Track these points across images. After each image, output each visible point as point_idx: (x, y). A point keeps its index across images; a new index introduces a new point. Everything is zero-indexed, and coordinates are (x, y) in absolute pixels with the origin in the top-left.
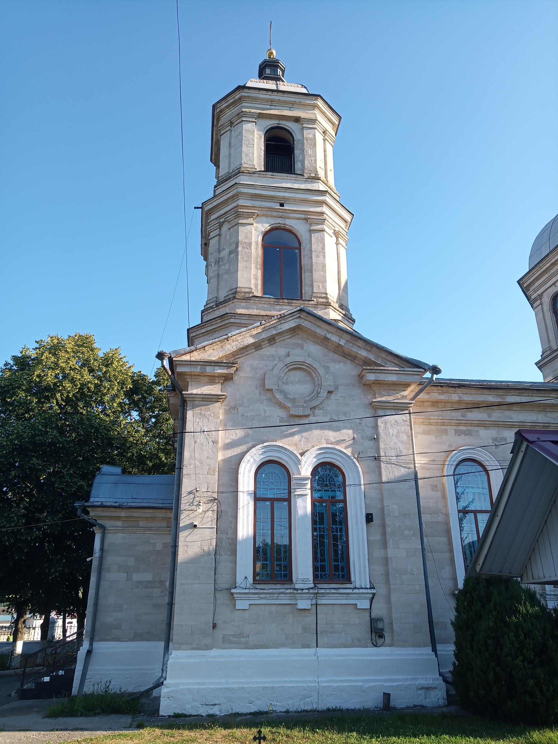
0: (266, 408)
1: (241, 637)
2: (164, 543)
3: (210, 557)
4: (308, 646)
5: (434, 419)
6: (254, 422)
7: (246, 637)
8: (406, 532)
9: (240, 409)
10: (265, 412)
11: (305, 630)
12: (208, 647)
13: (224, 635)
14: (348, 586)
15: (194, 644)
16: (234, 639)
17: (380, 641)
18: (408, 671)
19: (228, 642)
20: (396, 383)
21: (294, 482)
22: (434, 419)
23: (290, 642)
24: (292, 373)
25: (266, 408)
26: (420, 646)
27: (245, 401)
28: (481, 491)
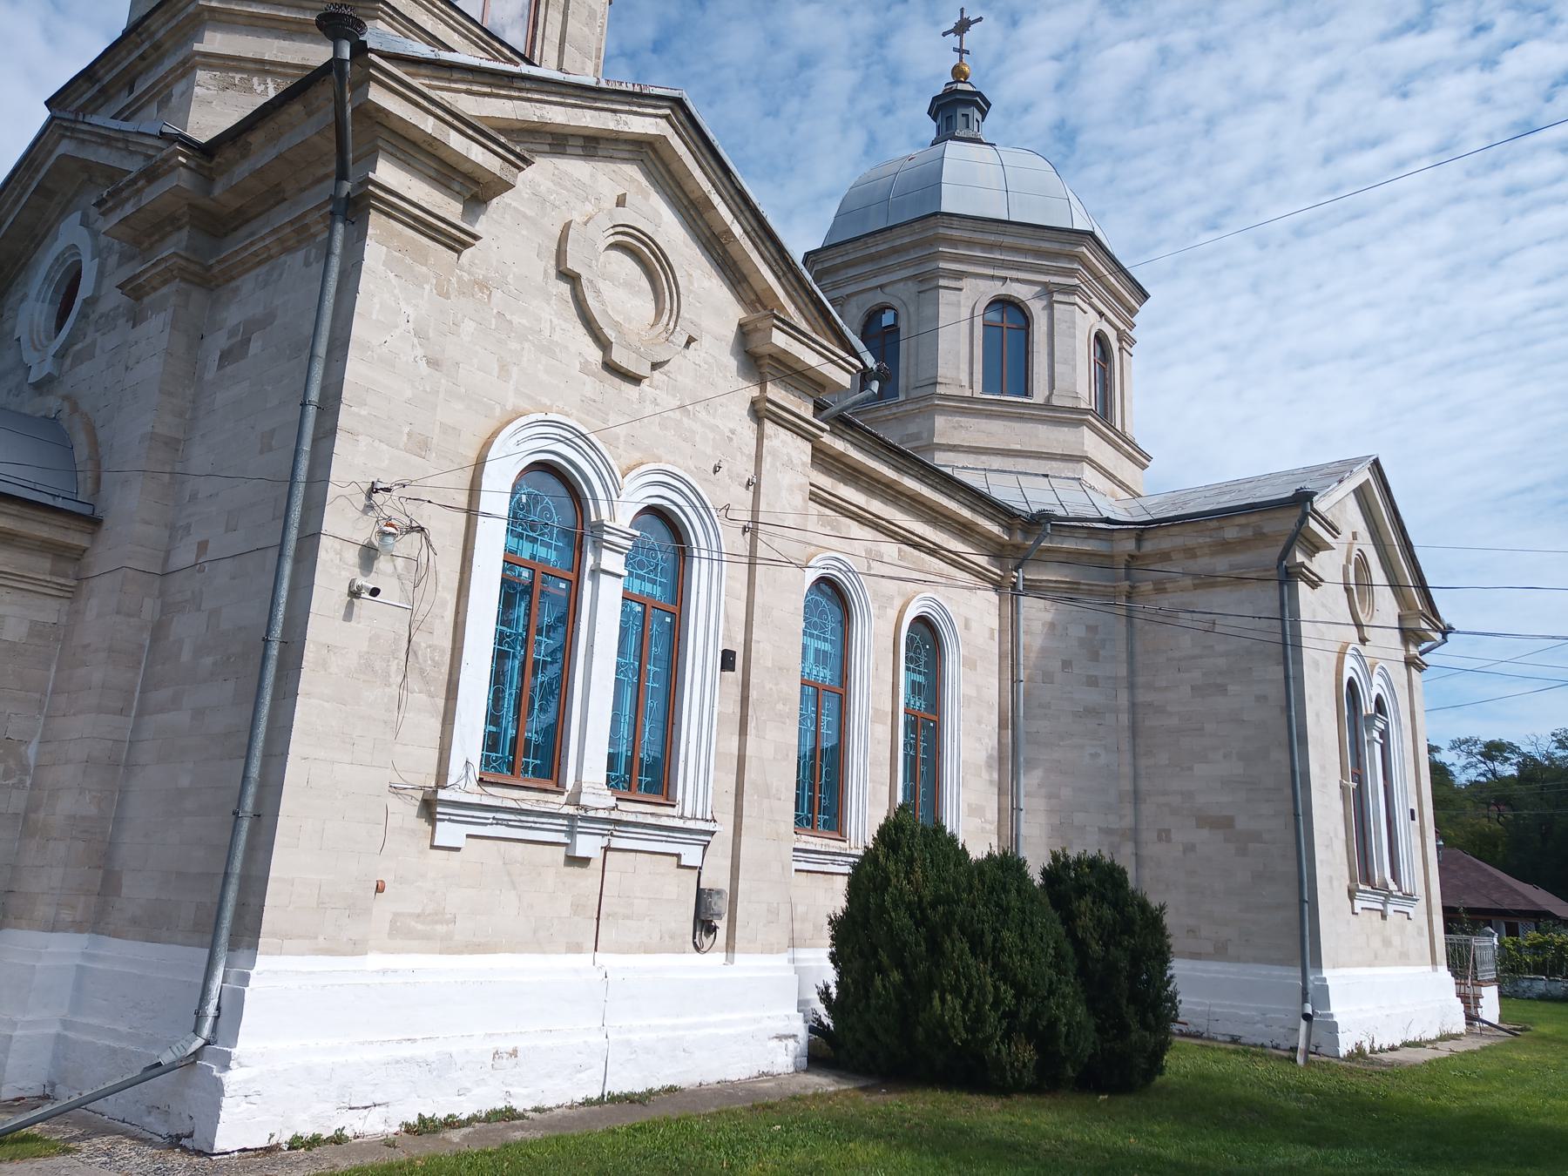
0: (555, 321)
1: (436, 922)
2: (34, 623)
3: (387, 690)
4: (576, 948)
5: (263, 238)
6: (526, 345)
7: (447, 922)
8: (780, 706)
9: (497, 294)
10: (553, 329)
11: (577, 908)
12: (357, 948)
13: (396, 914)
14: (669, 810)
15: (321, 938)
16: (420, 927)
17: (707, 942)
18: (742, 1011)
19: (403, 934)
20: (808, 373)
21: (339, 491)
22: (263, 238)
23: (536, 941)
24: (616, 255)
25: (555, 321)
26: (771, 952)
27: (510, 279)
28: (826, 647)
